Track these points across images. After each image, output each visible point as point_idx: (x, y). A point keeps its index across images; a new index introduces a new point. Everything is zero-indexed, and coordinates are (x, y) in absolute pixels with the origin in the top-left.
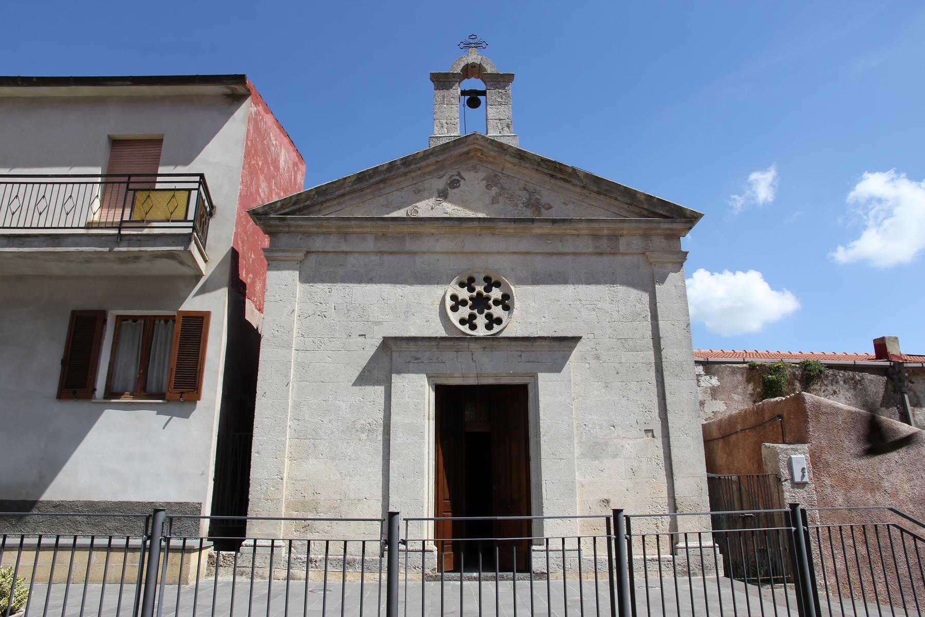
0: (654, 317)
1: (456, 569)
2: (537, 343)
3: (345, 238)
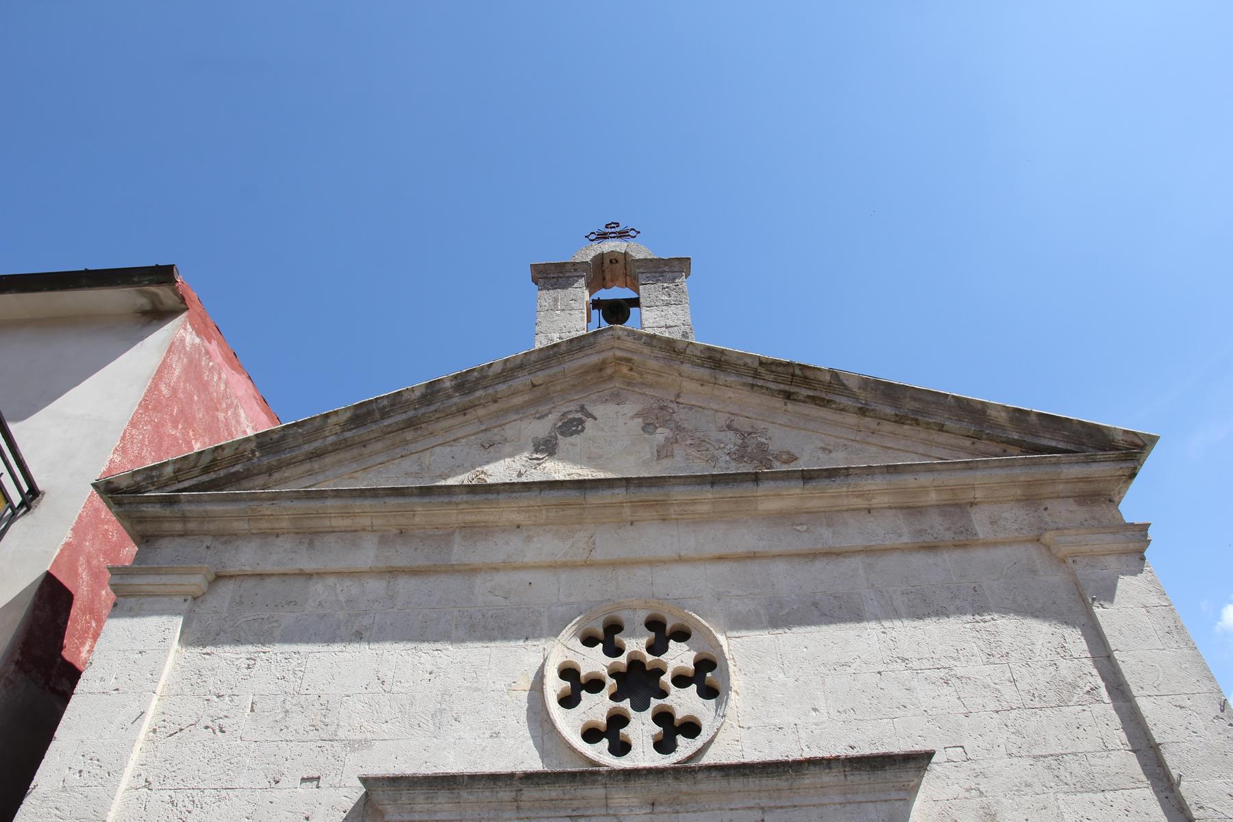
0: (1119, 689)
2: (807, 781)
3: (311, 544)
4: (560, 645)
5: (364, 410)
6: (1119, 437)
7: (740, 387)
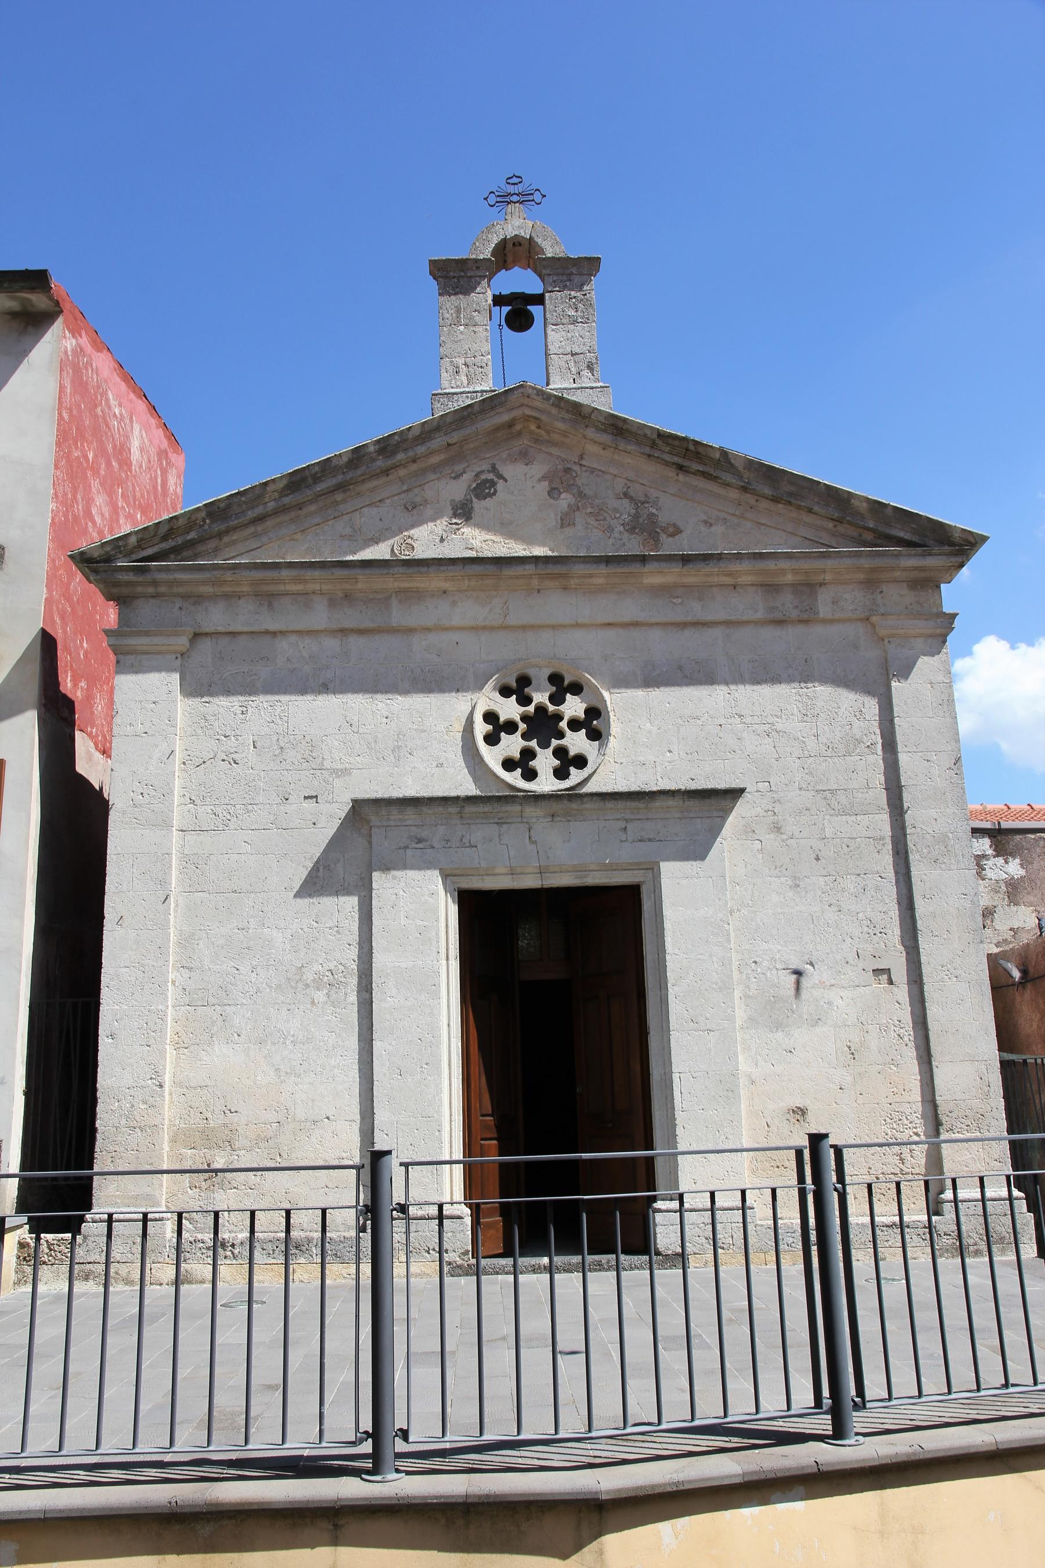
0: (890, 746)
1: (508, 1252)
2: (657, 804)
3: (270, 606)
4: (484, 697)
5: (299, 477)
6: (957, 535)
7: (638, 454)
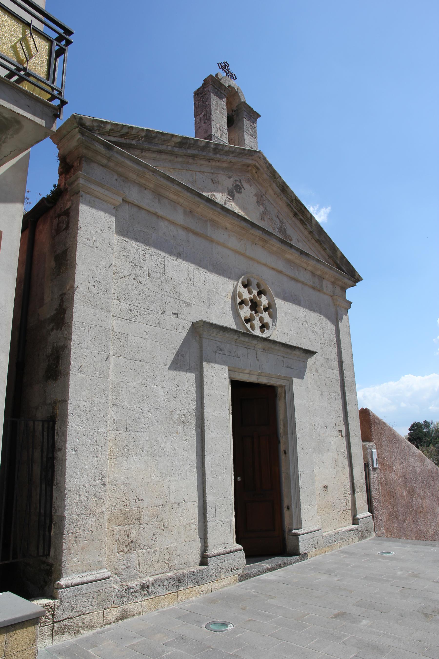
3: (159, 200)
6: (357, 276)
7: (285, 203)
